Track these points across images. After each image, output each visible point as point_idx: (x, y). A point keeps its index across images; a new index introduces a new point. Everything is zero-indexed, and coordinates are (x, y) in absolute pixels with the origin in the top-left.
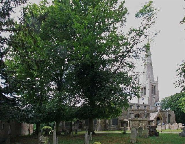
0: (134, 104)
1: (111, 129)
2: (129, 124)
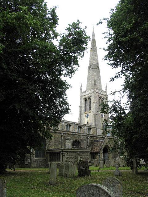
0: (74, 124)
1: (33, 165)
2: (61, 156)
